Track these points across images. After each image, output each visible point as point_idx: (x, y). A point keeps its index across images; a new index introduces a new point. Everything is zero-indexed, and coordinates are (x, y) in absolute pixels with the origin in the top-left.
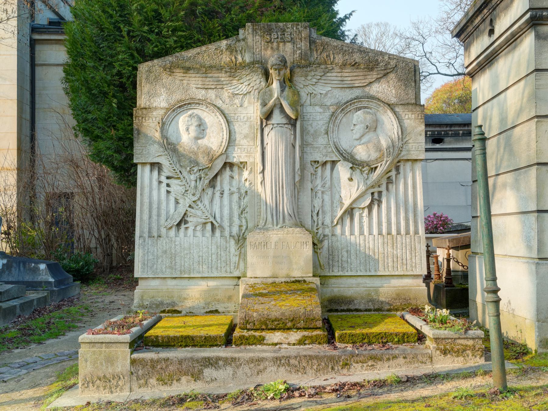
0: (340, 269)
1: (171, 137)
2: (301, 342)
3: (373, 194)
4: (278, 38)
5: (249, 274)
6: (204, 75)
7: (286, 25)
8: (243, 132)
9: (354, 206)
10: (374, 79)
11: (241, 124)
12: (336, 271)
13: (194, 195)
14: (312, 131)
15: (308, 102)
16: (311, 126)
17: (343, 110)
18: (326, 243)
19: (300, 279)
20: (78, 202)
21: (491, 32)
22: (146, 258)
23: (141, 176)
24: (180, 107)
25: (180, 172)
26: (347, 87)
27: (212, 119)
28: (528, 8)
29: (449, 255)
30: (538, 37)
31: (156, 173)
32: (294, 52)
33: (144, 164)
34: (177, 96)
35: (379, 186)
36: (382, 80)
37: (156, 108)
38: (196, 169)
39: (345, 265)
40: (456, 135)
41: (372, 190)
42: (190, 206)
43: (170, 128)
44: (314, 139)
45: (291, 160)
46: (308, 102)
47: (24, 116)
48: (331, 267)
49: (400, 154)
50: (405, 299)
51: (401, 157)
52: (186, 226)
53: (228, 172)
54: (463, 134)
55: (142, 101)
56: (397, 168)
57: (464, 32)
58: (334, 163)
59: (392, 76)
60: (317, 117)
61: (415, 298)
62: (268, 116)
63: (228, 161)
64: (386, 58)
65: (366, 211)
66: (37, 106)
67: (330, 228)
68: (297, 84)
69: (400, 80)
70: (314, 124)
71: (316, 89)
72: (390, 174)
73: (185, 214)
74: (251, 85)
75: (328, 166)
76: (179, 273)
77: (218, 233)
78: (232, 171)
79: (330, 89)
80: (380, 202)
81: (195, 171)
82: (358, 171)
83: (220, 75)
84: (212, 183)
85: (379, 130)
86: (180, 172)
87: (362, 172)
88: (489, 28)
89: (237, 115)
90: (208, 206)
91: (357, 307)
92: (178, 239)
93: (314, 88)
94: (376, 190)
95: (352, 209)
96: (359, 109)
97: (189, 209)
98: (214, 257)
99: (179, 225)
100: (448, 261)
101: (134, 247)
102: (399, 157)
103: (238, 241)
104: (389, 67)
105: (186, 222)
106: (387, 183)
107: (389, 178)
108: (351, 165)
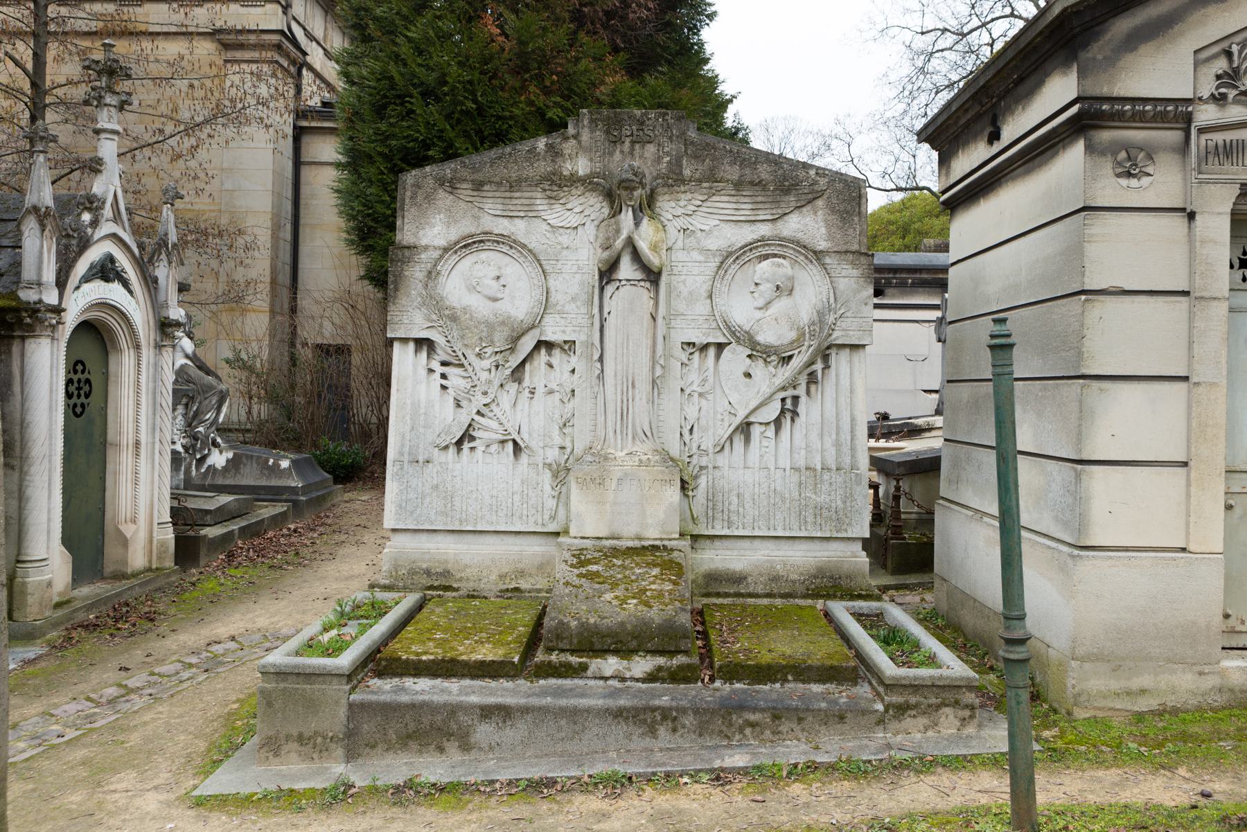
0: (726, 524)
2: (651, 678)
3: (783, 400)
4: (632, 135)
5: (573, 532)
6: (508, 194)
7: (646, 114)
9: (752, 419)
11: (567, 277)
12: (718, 527)
13: (485, 393)
18: (703, 481)
19: (657, 543)
20: (356, 359)
21: (995, 136)
24: (465, 246)
28: (1074, 95)
29: (898, 488)
30: (1090, 149)
31: (424, 354)
32: (658, 160)
33: (404, 340)
34: (466, 227)
35: (794, 388)
36: (804, 209)
37: (426, 248)
38: (489, 350)
39: (734, 518)
40: (902, 285)
41: (782, 394)
42: (479, 413)
46: (680, 244)
47: (281, 235)
48: (710, 520)
50: (832, 577)
54: (913, 283)
55: (406, 233)
56: (826, 358)
57: (944, 134)
58: (720, 347)
59: (820, 203)
60: (689, 273)
61: (849, 577)
62: (608, 273)
63: (543, 338)
64: (812, 172)
65: (772, 426)
66: (302, 221)
67: (711, 455)
68: (663, 213)
69: (833, 211)
70: (690, 280)
72: (814, 367)
73: (470, 425)
74: (586, 213)
75: (712, 352)
76: (457, 523)
77: (524, 458)
80: (795, 414)
82: (761, 361)
83: (534, 194)
84: (518, 373)
85: (796, 292)
88: (989, 129)
91: (751, 590)
92: (458, 466)
94: (790, 392)
95: (749, 424)
96: (766, 257)
97: (477, 418)
98: (517, 498)
99: (459, 443)
100: (896, 498)
101: (384, 472)
103: (555, 475)
104: (816, 188)
105: (472, 439)
106: (808, 383)
107: (811, 374)
108: (749, 352)
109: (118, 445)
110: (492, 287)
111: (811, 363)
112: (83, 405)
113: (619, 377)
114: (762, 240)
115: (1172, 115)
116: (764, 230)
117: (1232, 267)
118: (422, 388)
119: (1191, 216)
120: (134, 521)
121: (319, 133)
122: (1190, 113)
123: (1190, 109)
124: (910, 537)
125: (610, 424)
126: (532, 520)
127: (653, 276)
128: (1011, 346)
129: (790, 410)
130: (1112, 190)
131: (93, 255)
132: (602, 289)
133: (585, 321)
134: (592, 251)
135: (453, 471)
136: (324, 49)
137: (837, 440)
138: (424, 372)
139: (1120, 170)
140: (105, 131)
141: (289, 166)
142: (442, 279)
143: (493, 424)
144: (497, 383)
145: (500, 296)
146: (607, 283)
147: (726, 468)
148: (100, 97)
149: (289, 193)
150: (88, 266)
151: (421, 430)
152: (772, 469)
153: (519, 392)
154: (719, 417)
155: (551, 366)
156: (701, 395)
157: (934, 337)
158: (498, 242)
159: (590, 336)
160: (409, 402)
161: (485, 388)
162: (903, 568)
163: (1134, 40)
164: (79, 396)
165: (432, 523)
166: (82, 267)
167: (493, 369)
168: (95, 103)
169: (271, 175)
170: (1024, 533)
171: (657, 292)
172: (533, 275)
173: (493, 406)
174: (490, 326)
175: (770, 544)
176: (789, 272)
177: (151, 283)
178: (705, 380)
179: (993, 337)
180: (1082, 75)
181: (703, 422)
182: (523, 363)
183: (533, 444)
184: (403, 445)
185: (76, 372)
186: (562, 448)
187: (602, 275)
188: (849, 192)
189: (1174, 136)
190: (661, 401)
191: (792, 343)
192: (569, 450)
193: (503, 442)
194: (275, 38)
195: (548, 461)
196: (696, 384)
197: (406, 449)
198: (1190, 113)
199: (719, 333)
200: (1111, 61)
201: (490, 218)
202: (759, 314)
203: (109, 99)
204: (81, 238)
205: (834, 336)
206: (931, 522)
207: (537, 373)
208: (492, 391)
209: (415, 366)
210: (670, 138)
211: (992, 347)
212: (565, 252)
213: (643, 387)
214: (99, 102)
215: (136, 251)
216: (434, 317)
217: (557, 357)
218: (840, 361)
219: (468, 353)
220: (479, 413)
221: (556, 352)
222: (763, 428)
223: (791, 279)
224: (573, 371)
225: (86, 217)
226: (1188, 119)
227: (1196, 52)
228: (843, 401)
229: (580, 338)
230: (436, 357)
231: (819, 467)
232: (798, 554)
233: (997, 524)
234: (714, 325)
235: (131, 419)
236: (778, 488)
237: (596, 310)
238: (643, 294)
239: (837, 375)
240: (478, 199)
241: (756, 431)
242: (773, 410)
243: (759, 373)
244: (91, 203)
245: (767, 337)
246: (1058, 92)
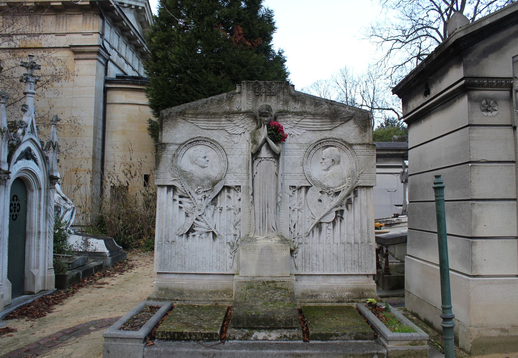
3: (336, 212)
5: (241, 274)
9: (322, 221)
13: (199, 210)
18: (300, 251)
21: (427, 93)
22: (163, 257)
24: (190, 143)
30: (470, 99)
31: (172, 192)
39: (315, 266)
42: (197, 219)
47: (98, 137)
52: (193, 234)
58: (307, 188)
62: (255, 155)
65: (332, 224)
66: (107, 130)
72: (350, 197)
73: (193, 225)
75: (303, 190)
77: (218, 240)
80: (342, 218)
82: (326, 195)
84: (214, 201)
85: (341, 163)
95: (321, 223)
96: (327, 146)
97: (196, 221)
98: (215, 258)
103: (232, 247)
105: (194, 231)
109: (31, 233)
111: (349, 195)
112: (16, 215)
113: (261, 202)
115: (504, 85)
116: (327, 135)
118: (170, 208)
119: (515, 128)
120: (38, 268)
121: (115, 90)
122: (512, 84)
123: (512, 82)
124: (394, 273)
125: (257, 223)
128: (443, 187)
129: (340, 215)
130: (481, 117)
131: (23, 148)
133: (245, 177)
134: (248, 144)
135: (185, 246)
136: (118, 53)
137: (361, 230)
138: (172, 201)
139: (483, 109)
140: (28, 93)
141: (102, 105)
142: (179, 158)
143: (204, 224)
144: (205, 205)
146: (255, 159)
148: (27, 78)
149: (101, 117)
150: (20, 153)
151: (170, 227)
152: (332, 243)
153: (215, 209)
154: (307, 220)
155: (230, 198)
156: (299, 210)
157: (400, 181)
158: (205, 141)
159: (248, 183)
160: (164, 214)
162: (393, 289)
163: (486, 53)
166: (17, 154)
167: (203, 199)
168: (25, 81)
169: (93, 109)
170: (450, 272)
171: (278, 163)
173: (203, 216)
174: (203, 180)
176: (338, 153)
177: (45, 159)
178: (301, 203)
179: (435, 183)
180: (465, 69)
181: (300, 222)
182: (217, 196)
183: (221, 233)
184: (162, 234)
185: (13, 200)
186: (235, 235)
187: (253, 155)
188: (363, 118)
189: (505, 93)
192: (238, 236)
193: (208, 232)
194: (97, 49)
195: (228, 241)
196: (296, 205)
197: (164, 236)
198: (512, 84)
199: (307, 182)
200: (477, 62)
201: (201, 130)
202: (324, 173)
203: (31, 79)
204: (18, 142)
205: (358, 182)
206: (403, 266)
207: (223, 201)
208: (203, 209)
209: (167, 198)
211: (435, 188)
212: (236, 145)
213: (272, 207)
214: (27, 80)
215: (40, 146)
216: (176, 175)
217: (232, 193)
218: (362, 193)
219: (192, 192)
221: (232, 191)
222: (327, 225)
223: (339, 157)
224: (240, 200)
225: (20, 131)
226: (511, 86)
227: (513, 57)
229: (243, 185)
230: (177, 194)
231: (353, 242)
233: (439, 268)
234: (304, 178)
235: (36, 221)
236: (334, 252)
237: (250, 172)
238: (272, 164)
239: (360, 200)
240: (196, 122)
241: (324, 226)
243: (325, 200)
244: (22, 125)
245: (329, 183)
246: (455, 75)
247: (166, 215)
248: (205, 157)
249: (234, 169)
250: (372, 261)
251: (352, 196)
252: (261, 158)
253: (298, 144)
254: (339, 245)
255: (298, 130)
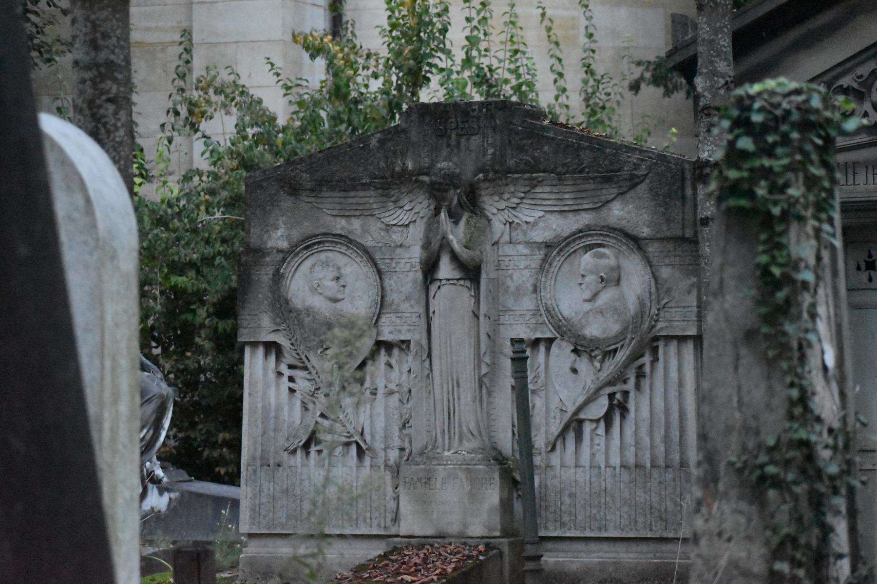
1: (293, 300)
3: (611, 396)
4: (457, 128)
8: (403, 289)
9: (582, 416)
10: (613, 196)
14: (512, 286)
15: (506, 237)
16: (512, 279)
17: (561, 250)
22: (257, 502)
23: (113, 381)
25: (306, 356)
26: (570, 211)
27: (355, 270)
31: (273, 358)
36: (628, 196)
39: (566, 518)
41: (609, 390)
42: (322, 415)
43: (293, 283)
44: (515, 301)
45: (472, 340)
49: (654, 326)
51: (656, 332)
52: (318, 448)
53: (383, 357)
56: (655, 351)
58: (550, 341)
60: (518, 265)
62: (430, 269)
63: (381, 338)
65: (602, 424)
67: (544, 454)
71: (520, 215)
72: (641, 361)
74: (416, 210)
75: (542, 348)
77: (367, 461)
78: (390, 355)
79: (541, 214)
81: (329, 357)
85: (623, 282)
86: (306, 356)
87: (592, 358)
89: (395, 261)
90: (351, 416)
93: (515, 213)
95: (581, 422)
96: (589, 248)
97: (320, 420)
99: (306, 446)
102: (654, 330)
105: (318, 442)
110: (330, 285)
114: (589, 228)
116: (586, 219)
117: (859, 268)
126: (375, 522)
127: (471, 273)
129: (619, 407)
132: (427, 290)
145: (340, 296)
146: (431, 283)
147: (558, 468)
152: (603, 466)
155: (391, 366)
160: (260, 405)
161: (326, 390)
164: (446, 558)
165: (283, 526)
171: (478, 289)
172: (370, 275)
175: (605, 546)
176: (612, 262)
190: (491, 400)
191: (616, 337)
192: (407, 451)
197: (259, 454)
202: (587, 306)
205: (658, 327)
209: (265, 369)
210: (494, 129)
212: (398, 251)
216: (278, 320)
220: (322, 415)
221: (396, 352)
224: (410, 371)
228: (673, 394)
230: (284, 360)
232: (631, 555)
238: (463, 296)
241: (587, 428)
242: (600, 407)
245: (593, 330)
247: (264, 407)
248: (338, 278)
249: (395, 302)
250: (253, 410)
251: (647, 359)
252: (441, 280)
253: (528, 243)
254: (618, 470)
255: (527, 212)
